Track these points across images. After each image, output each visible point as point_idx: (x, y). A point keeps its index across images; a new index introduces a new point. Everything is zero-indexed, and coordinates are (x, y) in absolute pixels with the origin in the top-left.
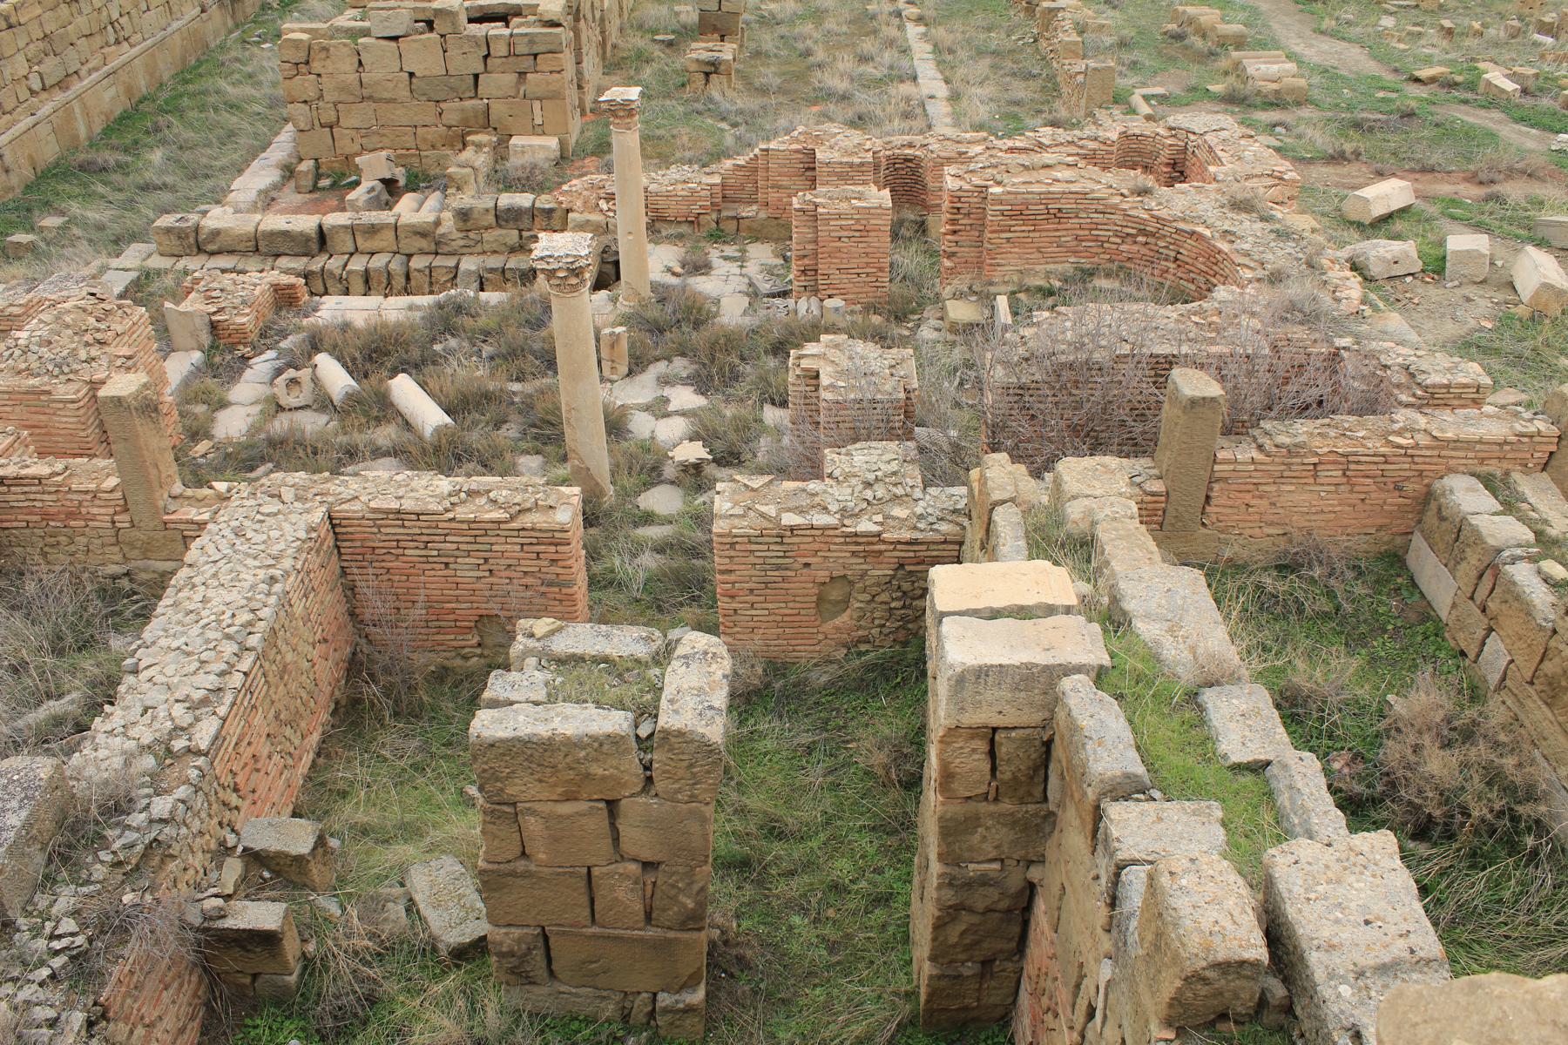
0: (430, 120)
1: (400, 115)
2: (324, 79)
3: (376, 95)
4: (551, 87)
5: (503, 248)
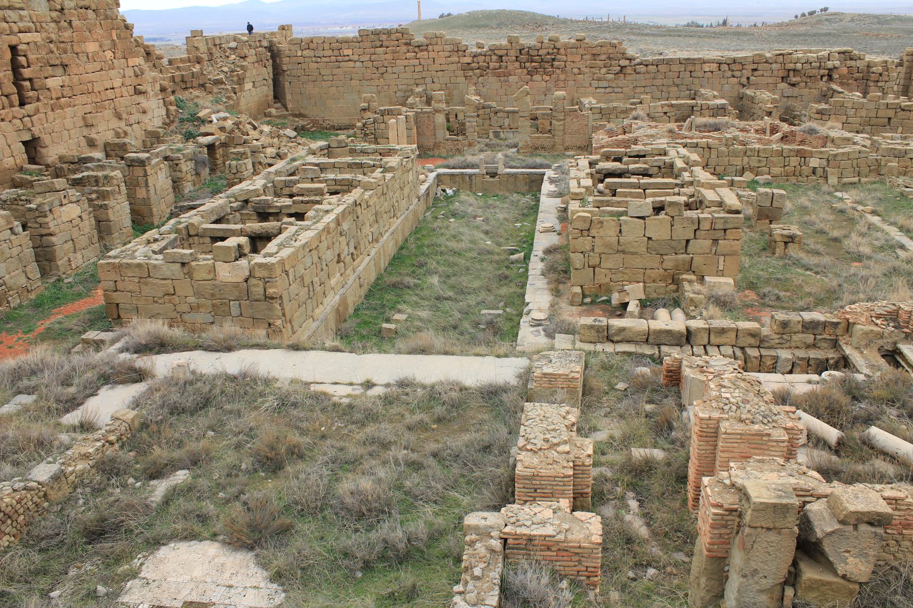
0: (656, 265)
1: (638, 262)
2: (597, 240)
3: (627, 250)
4: (733, 249)
5: (803, 345)
